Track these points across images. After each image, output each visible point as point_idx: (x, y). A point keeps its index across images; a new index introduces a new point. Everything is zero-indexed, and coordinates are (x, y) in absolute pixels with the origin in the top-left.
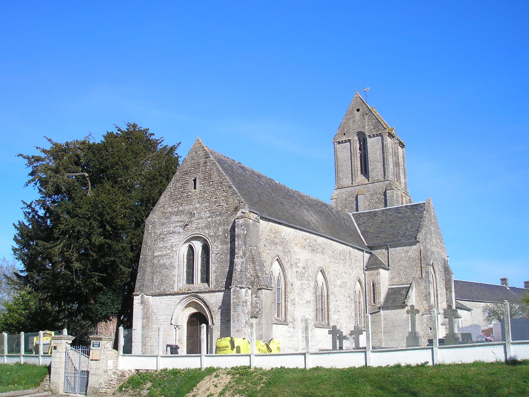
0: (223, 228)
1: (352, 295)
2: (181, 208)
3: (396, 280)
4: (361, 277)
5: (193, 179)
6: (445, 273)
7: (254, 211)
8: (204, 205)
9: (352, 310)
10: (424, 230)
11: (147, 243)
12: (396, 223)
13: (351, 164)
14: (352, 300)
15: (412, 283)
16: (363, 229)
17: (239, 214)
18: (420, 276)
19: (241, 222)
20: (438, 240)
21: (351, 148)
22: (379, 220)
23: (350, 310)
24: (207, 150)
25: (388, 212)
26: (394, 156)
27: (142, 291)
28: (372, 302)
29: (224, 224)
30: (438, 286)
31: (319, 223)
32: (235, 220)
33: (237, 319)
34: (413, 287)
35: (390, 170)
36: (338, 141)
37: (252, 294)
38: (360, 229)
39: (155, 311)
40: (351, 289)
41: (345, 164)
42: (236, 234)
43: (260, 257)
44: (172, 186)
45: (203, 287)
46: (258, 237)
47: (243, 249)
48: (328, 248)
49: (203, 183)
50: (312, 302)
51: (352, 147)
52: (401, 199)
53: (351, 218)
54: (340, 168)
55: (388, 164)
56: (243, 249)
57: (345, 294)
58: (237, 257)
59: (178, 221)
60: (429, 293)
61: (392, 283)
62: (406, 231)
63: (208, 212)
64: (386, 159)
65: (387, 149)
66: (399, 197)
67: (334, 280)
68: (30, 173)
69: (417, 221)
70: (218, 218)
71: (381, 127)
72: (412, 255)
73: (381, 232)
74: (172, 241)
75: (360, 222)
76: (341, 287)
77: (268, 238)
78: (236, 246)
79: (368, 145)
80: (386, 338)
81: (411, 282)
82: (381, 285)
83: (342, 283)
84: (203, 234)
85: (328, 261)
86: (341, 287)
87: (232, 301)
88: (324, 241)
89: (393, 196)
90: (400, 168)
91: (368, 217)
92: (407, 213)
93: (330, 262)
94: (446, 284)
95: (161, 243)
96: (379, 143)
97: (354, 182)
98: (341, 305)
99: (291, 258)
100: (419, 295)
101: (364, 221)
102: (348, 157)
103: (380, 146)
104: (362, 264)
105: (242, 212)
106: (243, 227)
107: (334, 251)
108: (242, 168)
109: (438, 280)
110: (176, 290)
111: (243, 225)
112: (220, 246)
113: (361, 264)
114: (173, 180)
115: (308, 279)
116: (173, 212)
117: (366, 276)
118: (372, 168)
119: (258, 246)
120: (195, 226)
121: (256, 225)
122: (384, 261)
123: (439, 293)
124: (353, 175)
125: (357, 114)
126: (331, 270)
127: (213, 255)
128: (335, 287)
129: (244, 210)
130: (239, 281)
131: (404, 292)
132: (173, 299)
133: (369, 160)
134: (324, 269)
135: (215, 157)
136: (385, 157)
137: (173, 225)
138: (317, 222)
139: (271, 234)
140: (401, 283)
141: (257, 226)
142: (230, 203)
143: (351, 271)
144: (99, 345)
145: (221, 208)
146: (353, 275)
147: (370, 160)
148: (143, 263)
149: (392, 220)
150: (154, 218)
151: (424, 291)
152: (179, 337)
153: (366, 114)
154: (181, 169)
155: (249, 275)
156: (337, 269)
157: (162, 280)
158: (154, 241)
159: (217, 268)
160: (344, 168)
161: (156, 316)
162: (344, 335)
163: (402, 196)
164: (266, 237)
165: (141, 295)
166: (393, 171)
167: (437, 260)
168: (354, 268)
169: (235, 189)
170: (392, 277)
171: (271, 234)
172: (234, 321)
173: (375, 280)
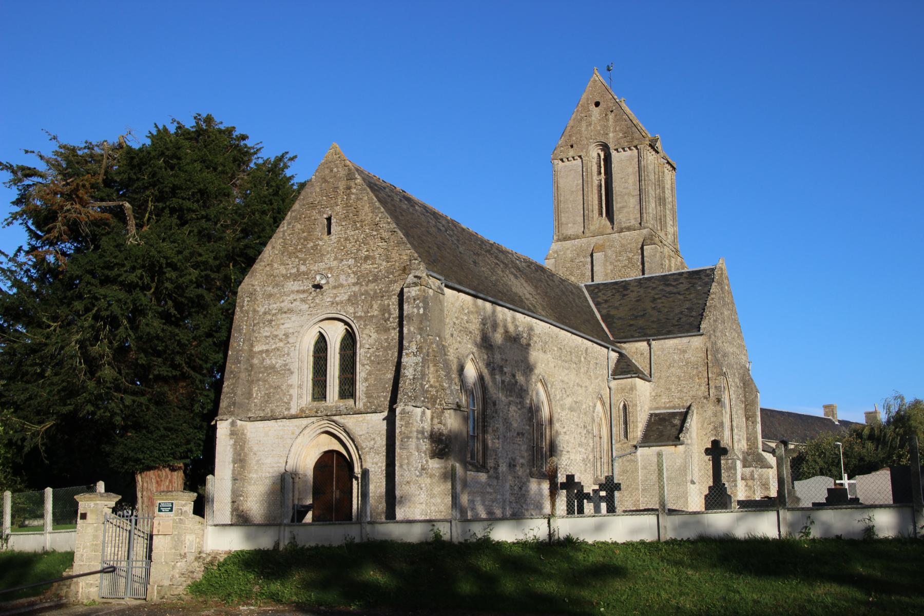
0: (380, 304)
1: (589, 424)
2: (303, 268)
3: (663, 401)
4: (604, 394)
5: (325, 216)
6: (744, 390)
7: (435, 275)
8: (345, 262)
9: (590, 449)
10: (713, 314)
11: (240, 329)
12: (662, 303)
13: (583, 198)
14: (589, 433)
15: (690, 406)
16: (604, 311)
17: (410, 279)
18: (707, 394)
19: (413, 294)
20: (734, 333)
21: (583, 170)
22: (634, 295)
23: (586, 450)
24: (350, 165)
25: (648, 282)
26: (657, 187)
27: (232, 414)
28: (622, 437)
29: (382, 297)
30: (734, 413)
31: (536, 299)
32: (402, 289)
33: (406, 461)
34: (693, 412)
35: (651, 211)
36: (559, 157)
37: (432, 419)
38: (599, 311)
39: (255, 449)
40: (588, 413)
41: (571, 199)
42: (405, 315)
43: (445, 355)
44: (285, 228)
45: (344, 407)
46: (442, 321)
47: (418, 340)
48: (552, 342)
49: (344, 224)
50: (526, 435)
51: (584, 169)
52: (667, 261)
53: (583, 292)
54: (562, 205)
55: (647, 200)
56: (418, 340)
57: (578, 423)
58: (407, 354)
59: (298, 291)
60: (722, 424)
61: (655, 405)
62: (681, 316)
63: (352, 276)
64: (643, 191)
65: (646, 173)
66: (664, 257)
67: (562, 397)
68: (14, 199)
69: (700, 299)
70: (371, 286)
71: (637, 135)
72: (693, 358)
73: (636, 317)
74: (286, 326)
75: (599, 300)
76: (571, 409)
77: (457, 322)
78: (405, 334)
79: (613, 166)
80: (646, 499)
81: (688, 404)
82: (639, 409)
83: (573, 403)
84: (345, 314)
85: (552, 365)
86: (571, 409)
87: (397, 431)
88: (546, 331)
89: (655, 255)
90: (667, 207)
91: (614, 291)
92: (681, 285)
93: (555, 367)
94: (746, 410)
95: (266, 329)
96: (633, 163)
97: (586, 230)
98: (572, 440)
99: (493, 358)
100: (702, 426)
101: (605, 298)
102: (577, 185)
103: (635, 168)
104: (605, 372)
105: (415, 277)
106: (418, 301)
107: (562, 348)
108: (409, 200)
109: (733, 402)
110: (293, 411)
111: (418, 299)
112: (374, 336)
113: (604, 372)
114: (288, 217)
115: (520, 394)
116: (289, 275)
117: (612, 392)
118: (619, 205)
119: (442, 335)
120: (328, 300)
121: (439, 299)
122: (642, 368)
123: (734, 424)
124: (585, 218)
125: (596, 111)
126: (556, 381)
127: (362, 350)
128: (563, 409)
129: (418, 273)
130: (411, 396)
131: (677, 421)
132: (288, 428)
133: (614, 192)
134: (546, 377)
135: (364, 179)
136: (643, 187)
137: (289, 298)
138: (533, 297)
139: (462, 316)
140: (672, 404)
141: (440, 301)
142: (394, 260)
143: (588, 383)
144: (172, 508)
145: (376, 268)
146: (590, 390)
147: (616, 193)
148: (234, 363)
149: (656, 296)
150: (253, 285)
151: (712, 419)
152: (299, 495)
153: (612, 111)
154: (303, 199)
155: (427, 386)
156: (566, 379)
157: (268, 395)
158: (254, 326)
159: (370, 374)
160: (570, 206)
161: (257, 459)
162: (585, 491)
163: (670, 256)
164: (454, 320)
165: (230, 420)
166: (655, 213)
167: (732, 367)
168: (593, 378)
169: (403, 236)
170: (657, 395)
171: (462, 316)
172: (401, 466)
173: (627, 399)
